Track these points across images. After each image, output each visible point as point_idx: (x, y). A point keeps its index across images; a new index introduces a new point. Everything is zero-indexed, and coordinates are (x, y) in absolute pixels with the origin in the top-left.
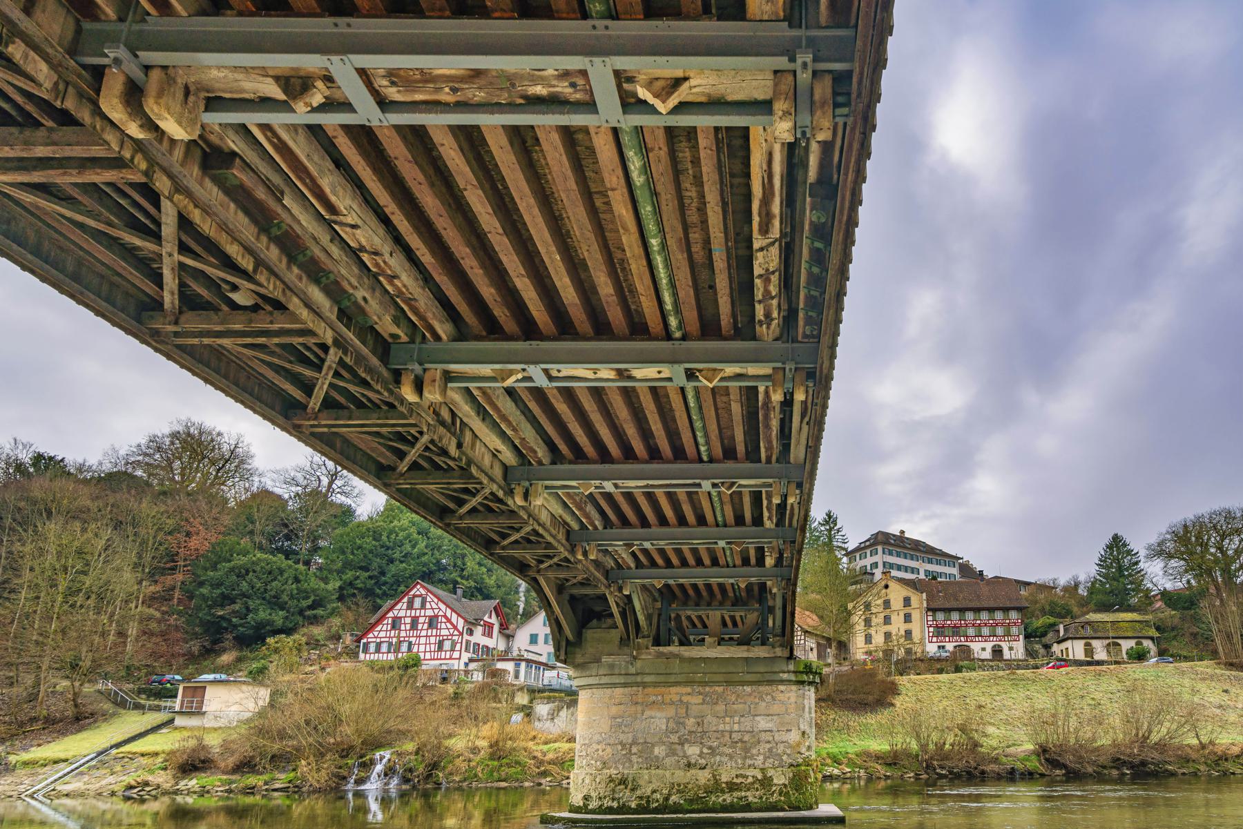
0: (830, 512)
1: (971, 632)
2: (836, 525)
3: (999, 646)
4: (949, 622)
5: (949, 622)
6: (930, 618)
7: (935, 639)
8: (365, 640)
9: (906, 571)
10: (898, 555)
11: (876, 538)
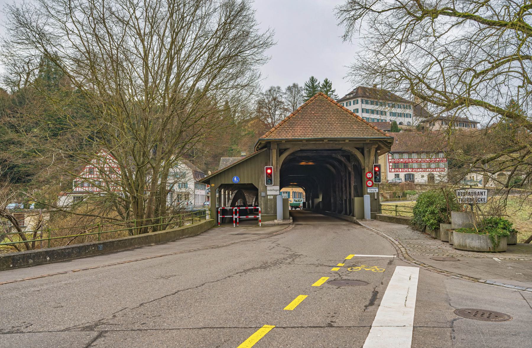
0: (327, 80)
1: (415, 165)
2: (331, 89)
3: (433, 174)
4: (402, 160)
5: (402, 160)
6: (390, 158)
7: (393, 170)
8: (75, 180)
9: (377, 114)
10: (372, 103)
11: (357, 92)
